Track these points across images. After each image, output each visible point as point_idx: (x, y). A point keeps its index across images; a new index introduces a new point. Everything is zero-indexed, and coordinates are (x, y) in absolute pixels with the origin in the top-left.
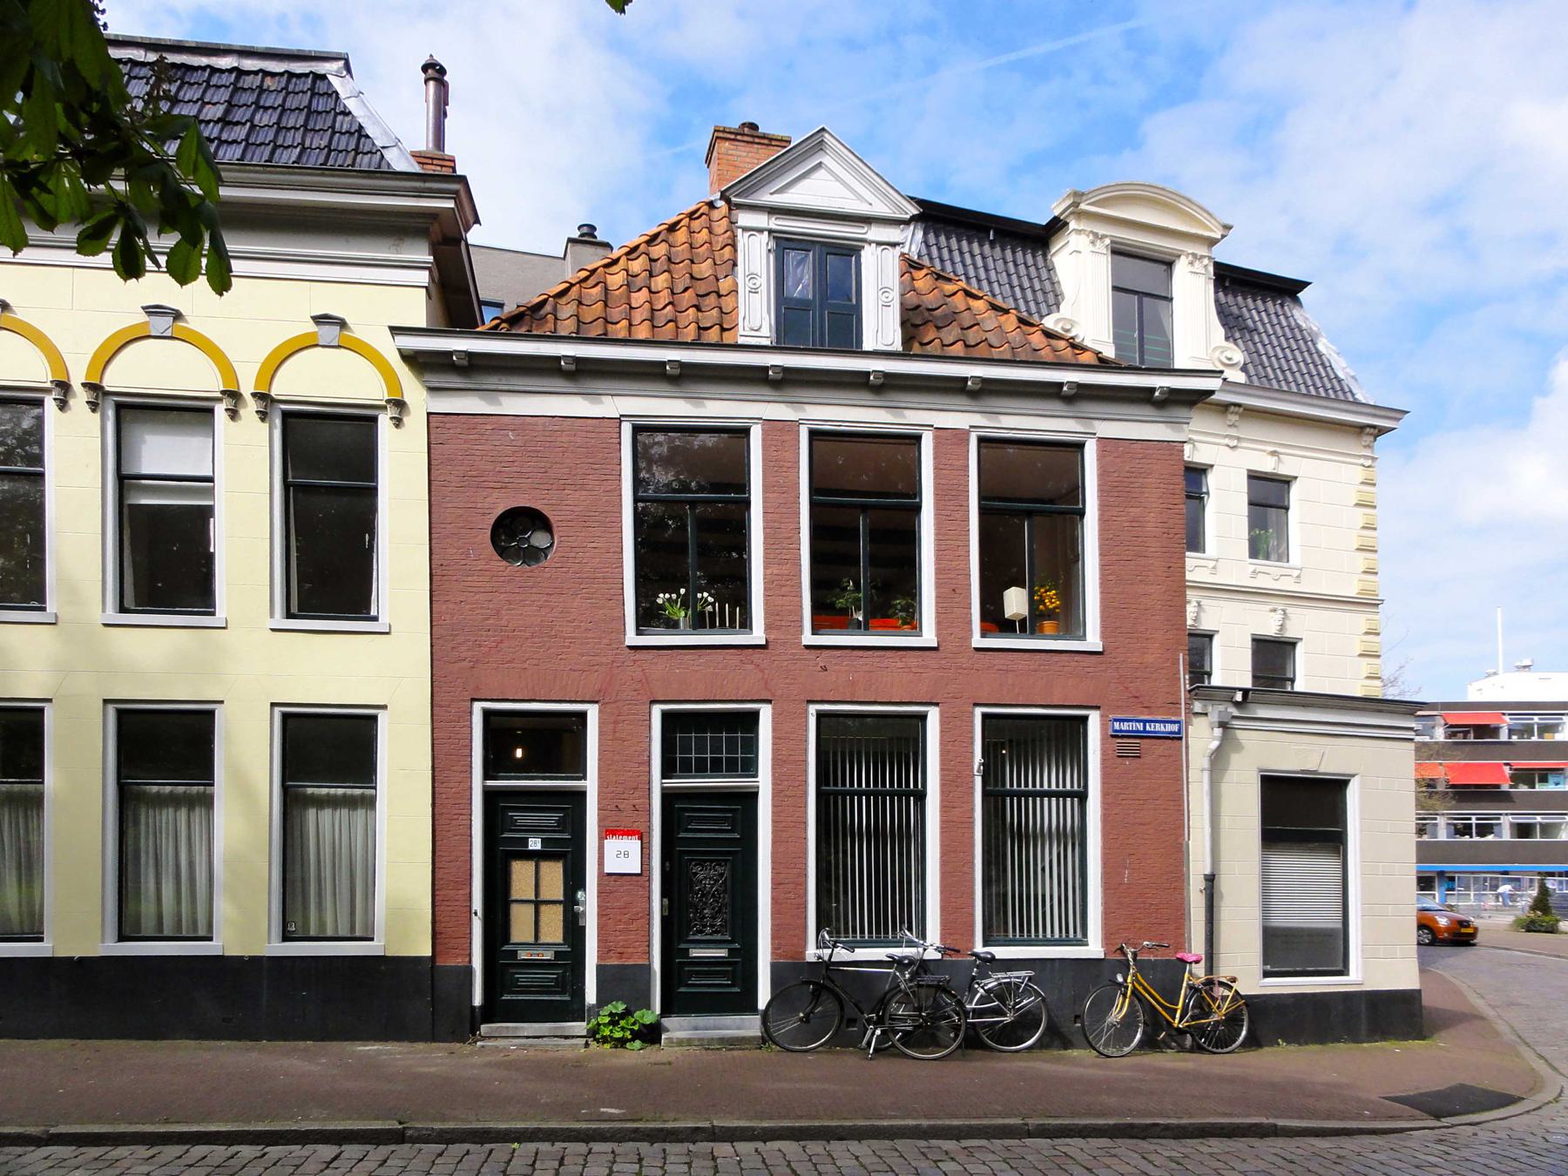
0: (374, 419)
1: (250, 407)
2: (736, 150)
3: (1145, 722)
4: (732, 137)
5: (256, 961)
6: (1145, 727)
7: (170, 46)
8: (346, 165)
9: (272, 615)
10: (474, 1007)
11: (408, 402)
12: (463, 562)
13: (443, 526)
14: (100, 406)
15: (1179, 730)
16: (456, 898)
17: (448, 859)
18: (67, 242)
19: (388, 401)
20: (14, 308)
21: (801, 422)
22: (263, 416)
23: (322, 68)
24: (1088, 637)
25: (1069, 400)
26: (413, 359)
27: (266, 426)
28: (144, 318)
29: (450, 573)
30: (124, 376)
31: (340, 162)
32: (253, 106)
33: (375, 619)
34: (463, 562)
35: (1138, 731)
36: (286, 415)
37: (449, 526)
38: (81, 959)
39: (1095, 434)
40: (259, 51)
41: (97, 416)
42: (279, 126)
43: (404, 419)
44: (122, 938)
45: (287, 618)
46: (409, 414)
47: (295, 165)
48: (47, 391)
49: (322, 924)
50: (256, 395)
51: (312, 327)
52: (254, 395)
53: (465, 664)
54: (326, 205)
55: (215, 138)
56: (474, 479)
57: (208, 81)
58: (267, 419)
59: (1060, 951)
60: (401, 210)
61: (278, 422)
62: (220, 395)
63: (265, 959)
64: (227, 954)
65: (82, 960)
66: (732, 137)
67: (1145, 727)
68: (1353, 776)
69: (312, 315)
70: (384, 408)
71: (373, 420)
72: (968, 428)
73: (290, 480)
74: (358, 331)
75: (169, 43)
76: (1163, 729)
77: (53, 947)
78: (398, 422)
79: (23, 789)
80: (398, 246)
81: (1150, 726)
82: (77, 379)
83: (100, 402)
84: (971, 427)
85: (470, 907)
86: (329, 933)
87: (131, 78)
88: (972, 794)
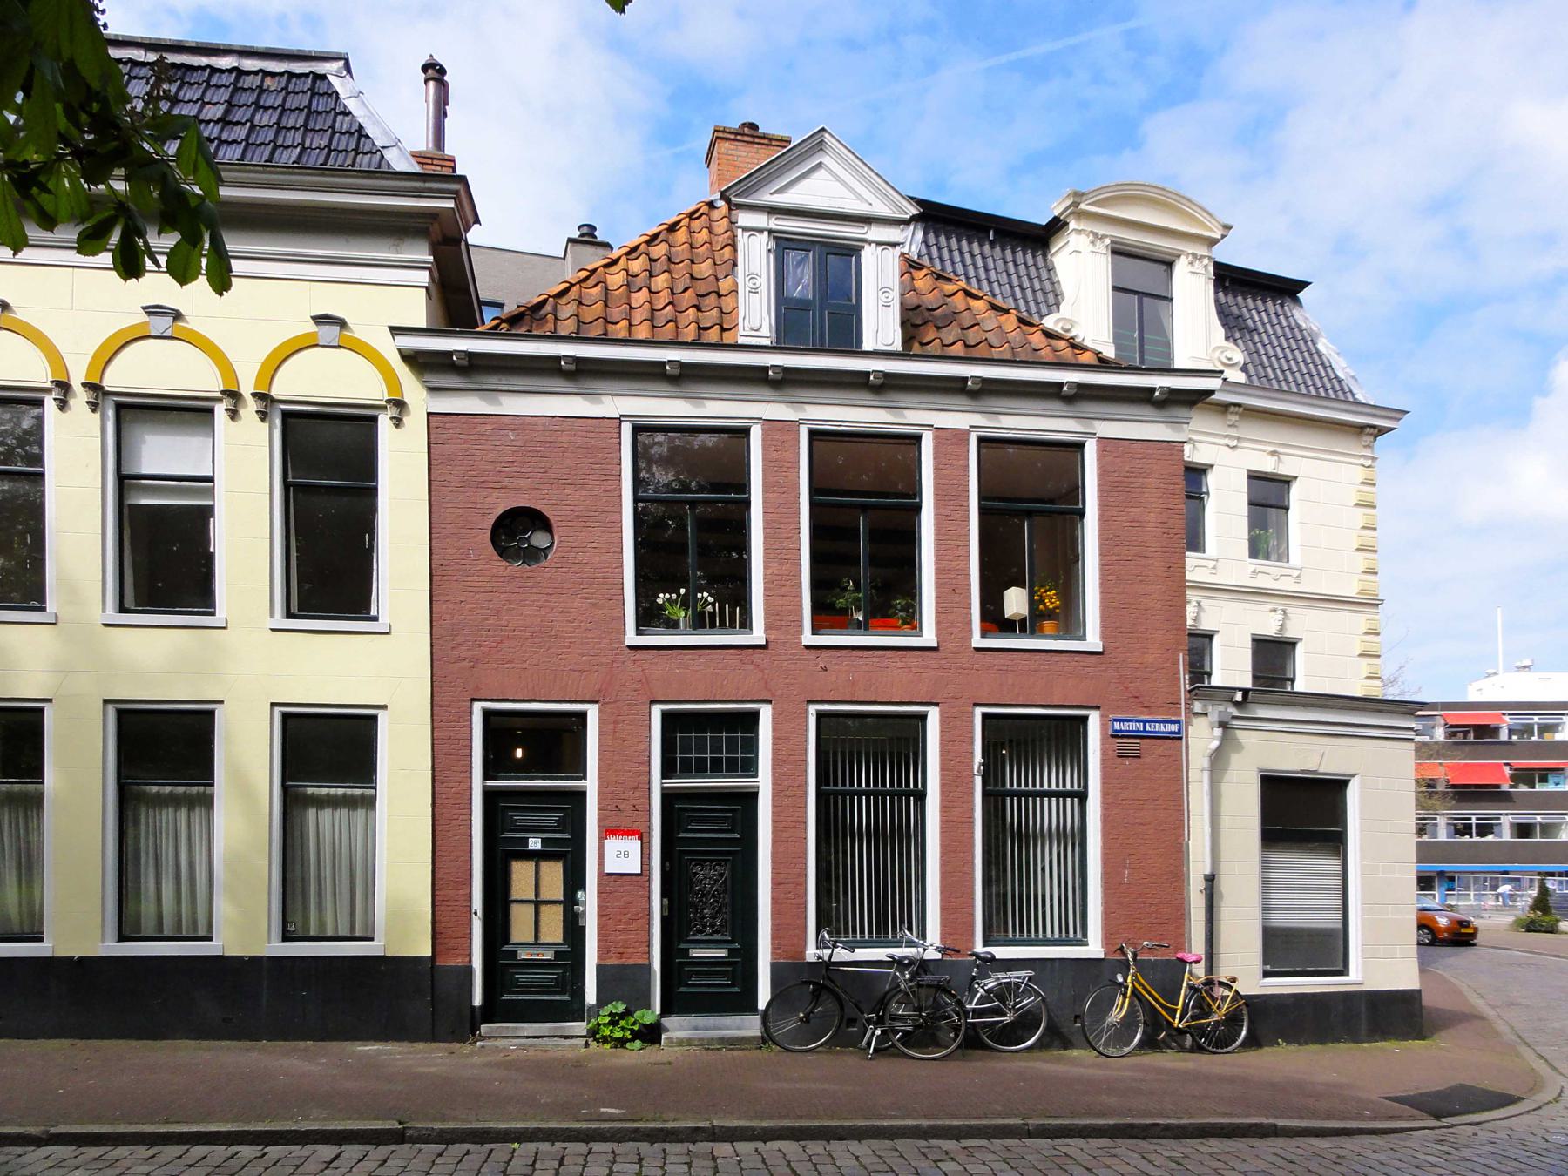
0: (374, 419)
1: (250, 407)
2: (736, 150)
3: (1145, 722)
4: (732, 137)
5: (256, 961)
6: (1145, 727)
7: (170, 46)
8: (346, 165)
9: (272, 615)
10: (474, 1007)
11: (408, 402)
12: (463, 562)
13: (443, 526)
14: (100, 406)
15: (1179, 730)
16: (456, 898)
17: (448, 859)
18: (67, 242)
19: (388, 401)
20: (14, 308)
21: (801, 422)
22: (263, 416)
23: (322, 68)
25: (1069, 400)
27: (266, 426)
28: (144, 318)
29: (450, 573)
30: (124, 376)
32: (253, 106)
33: (375, 619)
34: (463, 562)
36: (286, 415)
37: (449, 526)
39: (1095, 434)
40: (259, 51)
41: (97, 416)
42: (279, 126)
43: (404, 419)
44: (122, 938)
45: (287, 618)
46: (409, 414)
48: (47, 391)
51: (312, 327)
53: (465, 664)
54: (326, 205)
55: (215, 138)
56: (474, 479)
57: (208, 81)
58: (267, 419)
60: (401, 210)
61: (278, 422)
62: (220, 395)
63: (265, 959)
64: (227, 954)
65: (82, 960)
66: (732, 137)
67: (1145, 727)
69: (312, 315)
70: (384, 408)
71: (373, 420)
72: (968, 428)
73: (290, 480)
74: (358, 331)
75: (169, 43)
76: (1163, 729)
78: (398, 422)
80: (398, 246)
81: (1150, 726)
82: (77, 379)
83: (100, 402)
84: (971, 427)
86: (329, 933)
87: (131, 78)
88: (972, 794)
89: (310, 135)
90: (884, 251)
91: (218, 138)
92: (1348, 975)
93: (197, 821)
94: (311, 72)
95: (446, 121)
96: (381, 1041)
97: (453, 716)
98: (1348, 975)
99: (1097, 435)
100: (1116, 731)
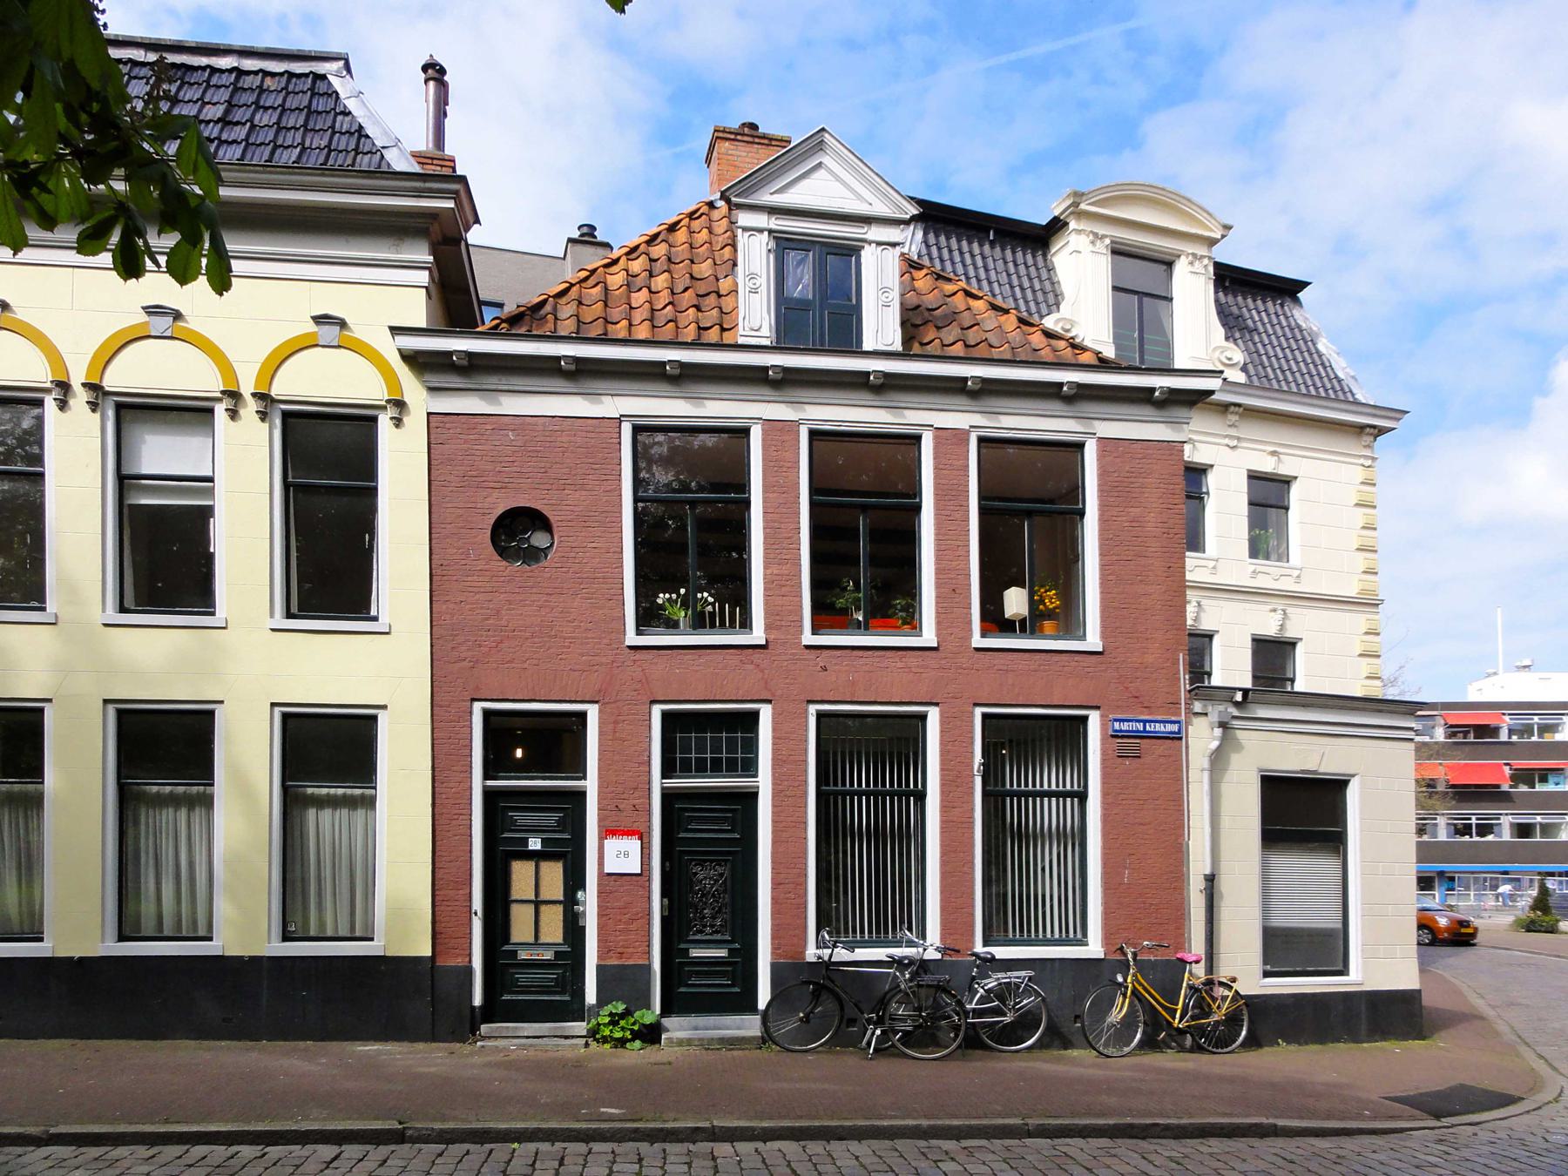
0: (374, 419)
1: (250, 407)
2: (736, 150)
3: (1145, 722)
4: (732, 137)
5: (256, 961)
6: (1145, 727)
7: (170, 46)
8: (346, 165)
9: (272, 615)
10: (474, 1007)
11: (408, 402)
12: (463, 562)
13: (443, 526)
14: (100, 406)
15: (1179, 730)
17: (448, 859)
18: (67, 242)
19: (388, 401)
20: (14, 308)
21: (801, 422)
22: (263, 416)
24: (1088, 637)
25: (1069, 400)
27: (266, 426)
28: (144, 318)
29: (450, 573)
30: (124, 376)
32: (253, 106)
33: (375, 619)
34: (463, 562)
35: (1138, 731)
37: (449, 526)
38: (81, 959)
39: (1095, 434)
40: (259, 51)
41: (97, 416)
42: (279, 126)
43: (404, 419)
44: (122, 938)
45: (287, 618)
46: (409, 414)
48: (47, 391)
51: (312, 327)
52: (254, 395)
53: (465, 664)
54: (326, 205)
55: (215, 138)
56: (474, 479)
57: (208, 81)
58: (267, 419)
59: (1060, 951)
60: (401, 210)
61: (278, 422)
62: (220, 395)
63: (265, 959)
64: (227, 954)
65: (82, 960)
66: (732, 137)
67: (1145, 727)
68: (1353, 776)
69: (312, 315)
70: (384, 408)
71: (373, 420)
72: (968, 428)
73: (290, 480)
74: (358, 331)
75: (169, 43)
76: (1163, 729)
77: (53, 947)
78: (398, 422)
79: (23, 789)
80: (398, 246)
81: (1150, 726)
82: (77, 379)
83: (100, 402)
84: (971, 427)
86: (329, 933)
87: (131, 78)
89: (310, 135)
90: (884, 251)
91: (218, 138)
93: (197, 821)
94: (311, 72)
95: (446, 121)
99: (1097, 435)
100: (1116, 731)
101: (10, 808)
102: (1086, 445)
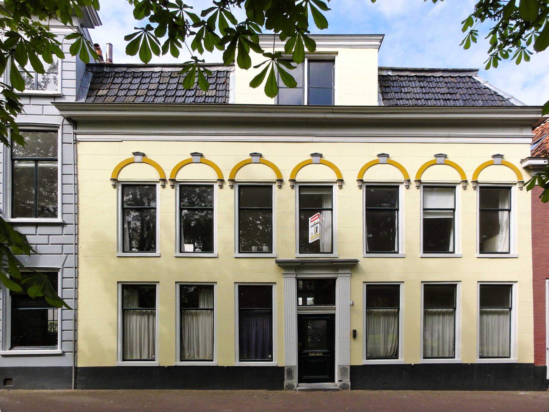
0: (271, 187)
1: (227, 184)
5: (472, 365)
7: (420, 70)
8: (161, 102)
9: (235, 252)
10: (547, 380)
11: (284, 180)
12: (542, 234)
13: (535, 222)
14: (175, 186)
16: (541, 344)
17: (538, 331)
18: (444, 135)
19: (160, 180)
20: (390, 157)
22: (232, 187)
23: (470, 74)
24: (511, 253)
26: (527, 168)
27: (116, 190)
28: (191, 157)
29: (537, 237)
30: (429, 177)
31: (169, 101)
32: (177, 84)
33: (398, 253)
34: (542, 234)
36: (481, 187)
37: (537, 222)
38: (415, 365)
40: (450, 70)
41: (116, 190)
42: (196, 89)
43: (166, 186)
44: (181, 360)
45: (239, 253)
46: (345, 184)
47: (183, 103)
48: (403, 183)
49: (488, 353)
50: (229, 180)
51: (250, 157)
52: (169, 180)
53: (544, 267)
54: (104, 116)
55: (214, 96)
56: (547, 206)
57: (151, 76)
58: (419, 188)
59: (246, 364)
60: (375, 118)
61: (178, 188)
62: (217, 181)
63: (476, 365)
64: (219, 365)
65: (228, 368)
69: (133, 152)
70: (275, 183)
71: (271, 187)
73: (182, 207)
74: (507, 159)
75: (419, 69)
77: (404, 361)
78: (280, 187)
79: (442, 311)
80: (521, 130)
82: (226, 178)
83: (234, 185)
85: (545, 347)
86: (441, 356)
87: (208, 78)
89: (218, 92)
91: (205, 95)
92: (397, 358)
93: (201, 320)
94: (142, 71)
96: (529, 391)
97: (539, 284)
98: (397, 358)
101: (429, 316)
102: (333, 187)
